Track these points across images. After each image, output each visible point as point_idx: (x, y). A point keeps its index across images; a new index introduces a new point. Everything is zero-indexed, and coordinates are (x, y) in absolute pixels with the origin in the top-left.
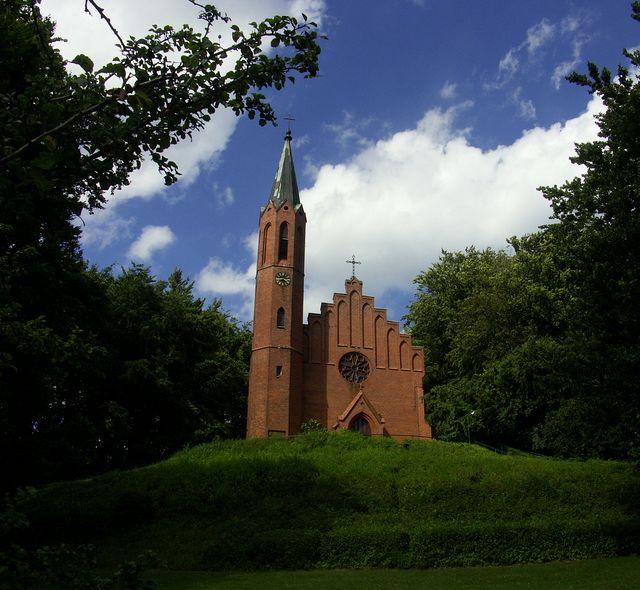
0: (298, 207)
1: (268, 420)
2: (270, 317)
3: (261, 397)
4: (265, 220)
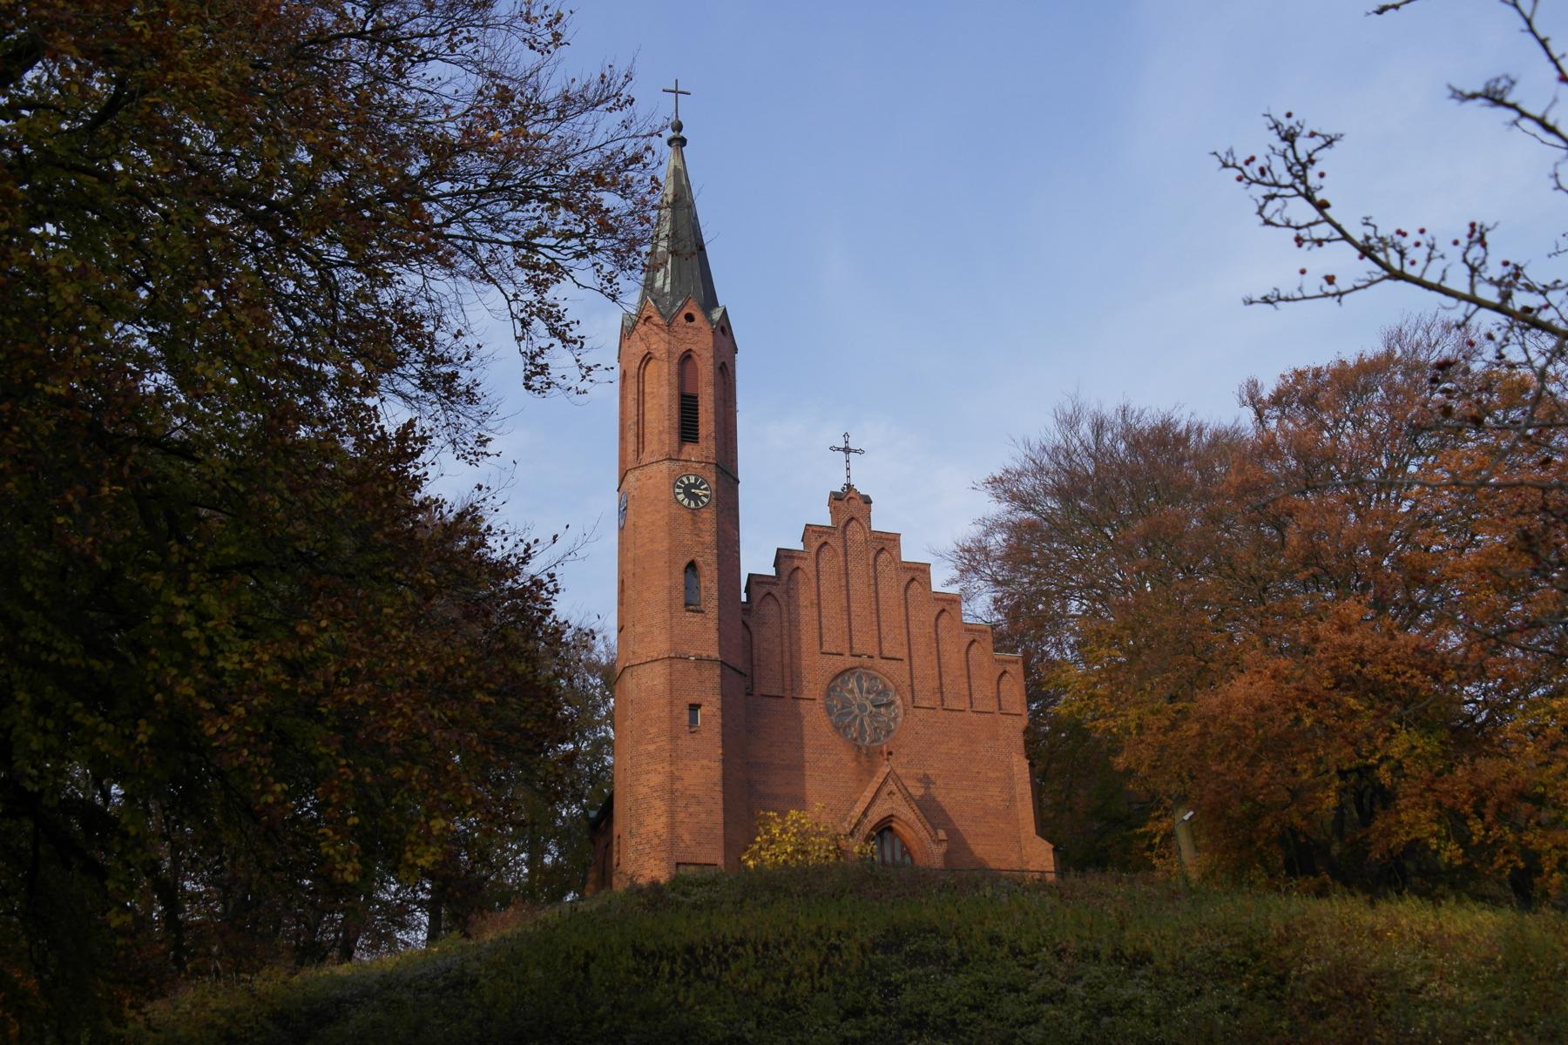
0: (716, 315)
2: (661, 586)
3: (655, 779)
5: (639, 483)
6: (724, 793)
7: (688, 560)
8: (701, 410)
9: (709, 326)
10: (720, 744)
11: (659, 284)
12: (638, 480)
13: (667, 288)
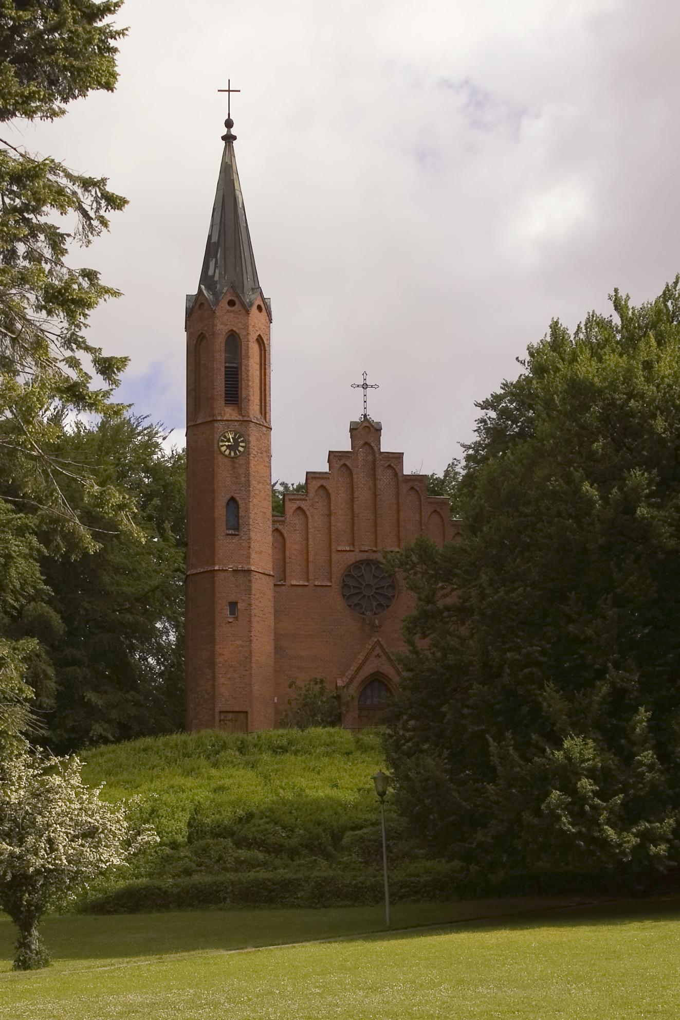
7: (228, 497)
11: (211, 273)
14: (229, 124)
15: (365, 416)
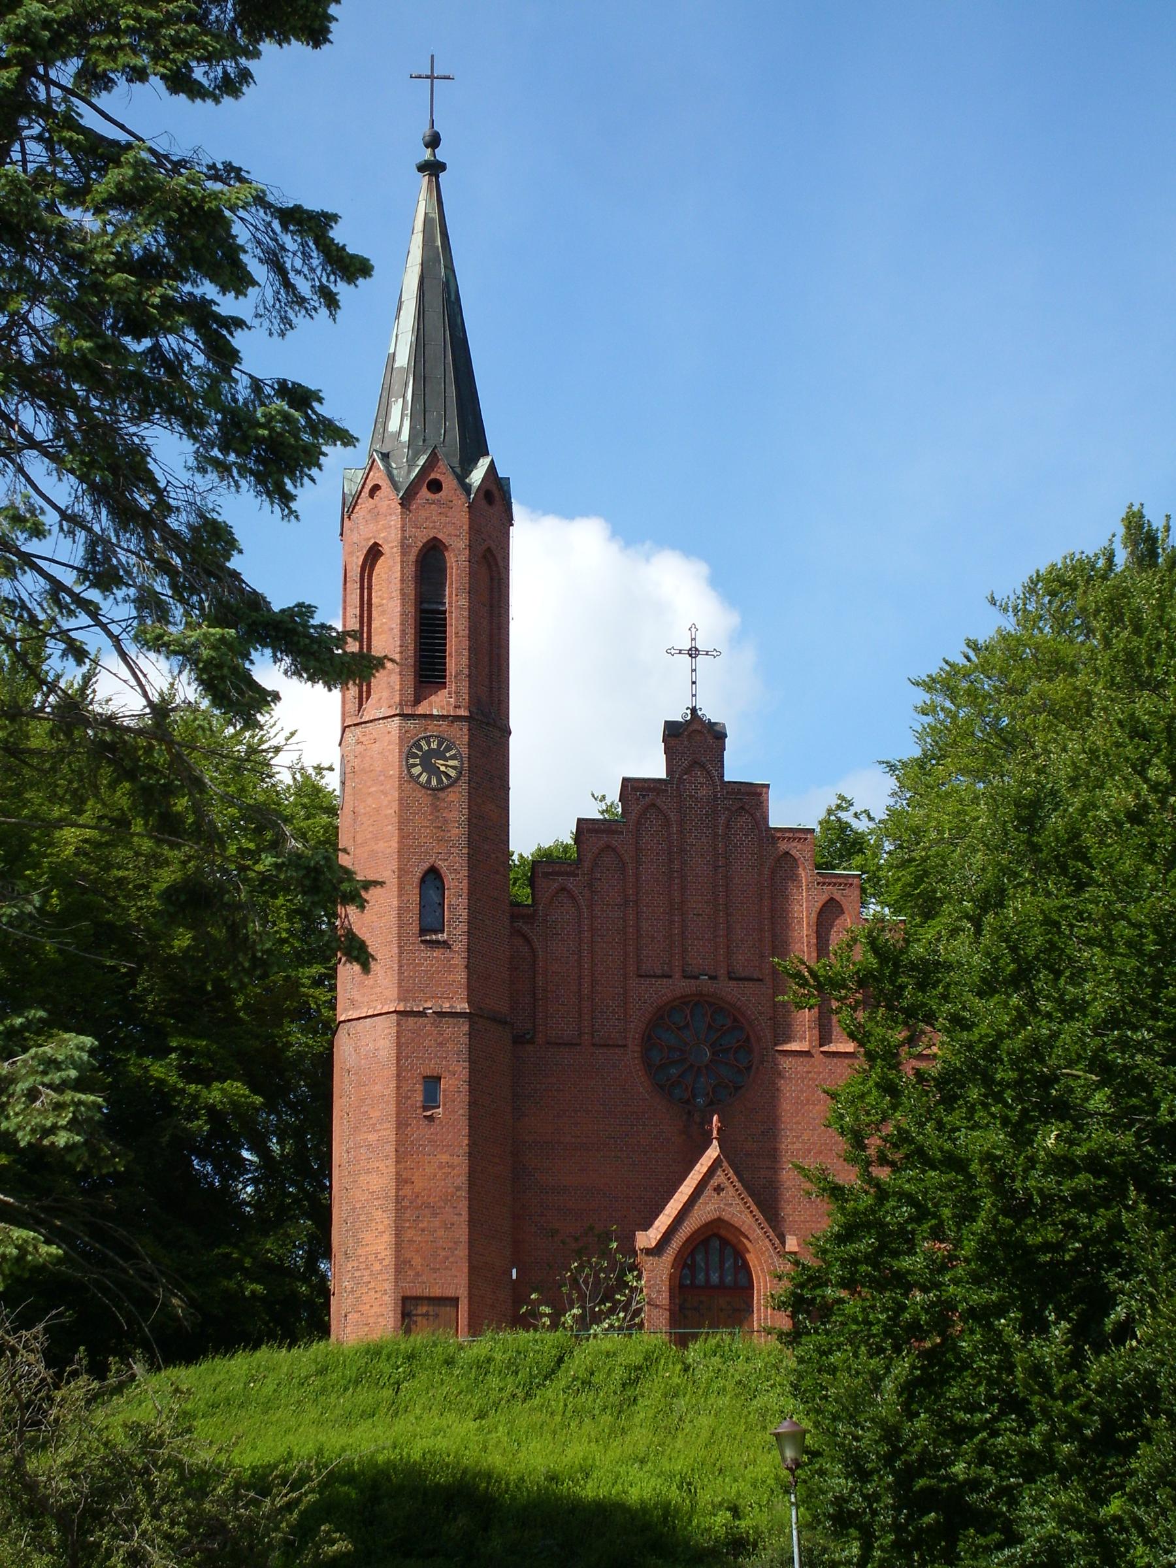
0: (477, 476)
1: (401, 1266)
4: (364, 531)
5: (360, 748)
6: (470, 1199)
7: (426, 866)
8: (451, 631)
9: (463, 497)
10: (466, 1131)
11: (393, 426)
12: (359, 742)
13: (405, 436)
14: (434, 141)
15: (694, 710)
